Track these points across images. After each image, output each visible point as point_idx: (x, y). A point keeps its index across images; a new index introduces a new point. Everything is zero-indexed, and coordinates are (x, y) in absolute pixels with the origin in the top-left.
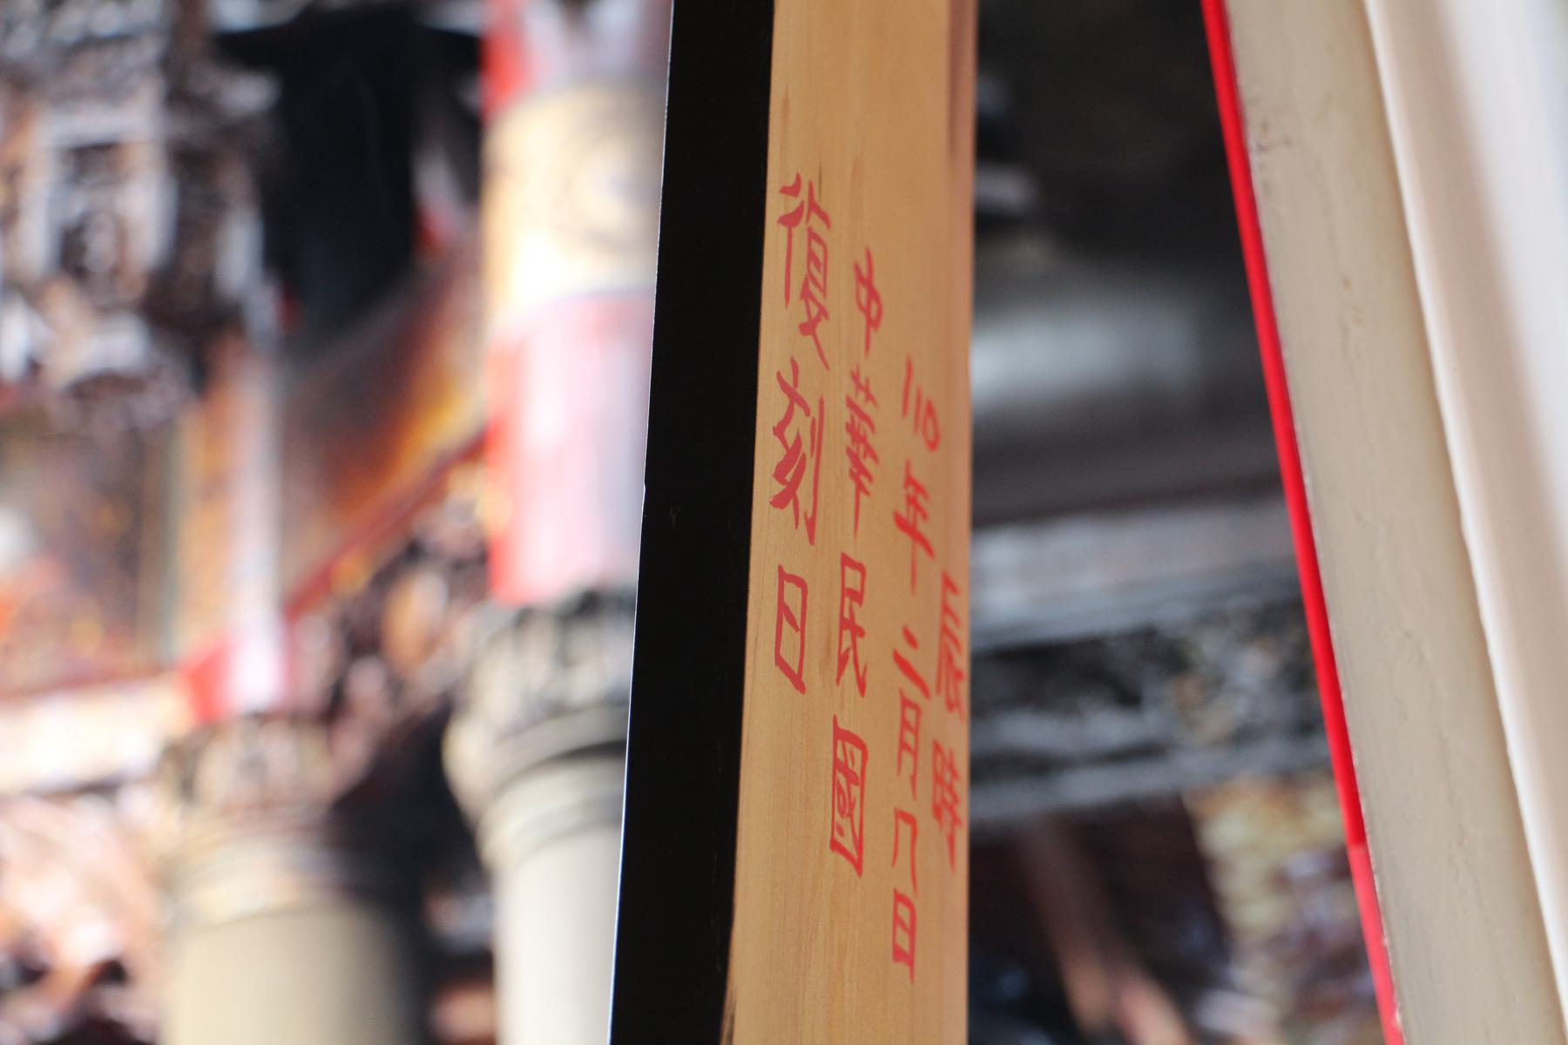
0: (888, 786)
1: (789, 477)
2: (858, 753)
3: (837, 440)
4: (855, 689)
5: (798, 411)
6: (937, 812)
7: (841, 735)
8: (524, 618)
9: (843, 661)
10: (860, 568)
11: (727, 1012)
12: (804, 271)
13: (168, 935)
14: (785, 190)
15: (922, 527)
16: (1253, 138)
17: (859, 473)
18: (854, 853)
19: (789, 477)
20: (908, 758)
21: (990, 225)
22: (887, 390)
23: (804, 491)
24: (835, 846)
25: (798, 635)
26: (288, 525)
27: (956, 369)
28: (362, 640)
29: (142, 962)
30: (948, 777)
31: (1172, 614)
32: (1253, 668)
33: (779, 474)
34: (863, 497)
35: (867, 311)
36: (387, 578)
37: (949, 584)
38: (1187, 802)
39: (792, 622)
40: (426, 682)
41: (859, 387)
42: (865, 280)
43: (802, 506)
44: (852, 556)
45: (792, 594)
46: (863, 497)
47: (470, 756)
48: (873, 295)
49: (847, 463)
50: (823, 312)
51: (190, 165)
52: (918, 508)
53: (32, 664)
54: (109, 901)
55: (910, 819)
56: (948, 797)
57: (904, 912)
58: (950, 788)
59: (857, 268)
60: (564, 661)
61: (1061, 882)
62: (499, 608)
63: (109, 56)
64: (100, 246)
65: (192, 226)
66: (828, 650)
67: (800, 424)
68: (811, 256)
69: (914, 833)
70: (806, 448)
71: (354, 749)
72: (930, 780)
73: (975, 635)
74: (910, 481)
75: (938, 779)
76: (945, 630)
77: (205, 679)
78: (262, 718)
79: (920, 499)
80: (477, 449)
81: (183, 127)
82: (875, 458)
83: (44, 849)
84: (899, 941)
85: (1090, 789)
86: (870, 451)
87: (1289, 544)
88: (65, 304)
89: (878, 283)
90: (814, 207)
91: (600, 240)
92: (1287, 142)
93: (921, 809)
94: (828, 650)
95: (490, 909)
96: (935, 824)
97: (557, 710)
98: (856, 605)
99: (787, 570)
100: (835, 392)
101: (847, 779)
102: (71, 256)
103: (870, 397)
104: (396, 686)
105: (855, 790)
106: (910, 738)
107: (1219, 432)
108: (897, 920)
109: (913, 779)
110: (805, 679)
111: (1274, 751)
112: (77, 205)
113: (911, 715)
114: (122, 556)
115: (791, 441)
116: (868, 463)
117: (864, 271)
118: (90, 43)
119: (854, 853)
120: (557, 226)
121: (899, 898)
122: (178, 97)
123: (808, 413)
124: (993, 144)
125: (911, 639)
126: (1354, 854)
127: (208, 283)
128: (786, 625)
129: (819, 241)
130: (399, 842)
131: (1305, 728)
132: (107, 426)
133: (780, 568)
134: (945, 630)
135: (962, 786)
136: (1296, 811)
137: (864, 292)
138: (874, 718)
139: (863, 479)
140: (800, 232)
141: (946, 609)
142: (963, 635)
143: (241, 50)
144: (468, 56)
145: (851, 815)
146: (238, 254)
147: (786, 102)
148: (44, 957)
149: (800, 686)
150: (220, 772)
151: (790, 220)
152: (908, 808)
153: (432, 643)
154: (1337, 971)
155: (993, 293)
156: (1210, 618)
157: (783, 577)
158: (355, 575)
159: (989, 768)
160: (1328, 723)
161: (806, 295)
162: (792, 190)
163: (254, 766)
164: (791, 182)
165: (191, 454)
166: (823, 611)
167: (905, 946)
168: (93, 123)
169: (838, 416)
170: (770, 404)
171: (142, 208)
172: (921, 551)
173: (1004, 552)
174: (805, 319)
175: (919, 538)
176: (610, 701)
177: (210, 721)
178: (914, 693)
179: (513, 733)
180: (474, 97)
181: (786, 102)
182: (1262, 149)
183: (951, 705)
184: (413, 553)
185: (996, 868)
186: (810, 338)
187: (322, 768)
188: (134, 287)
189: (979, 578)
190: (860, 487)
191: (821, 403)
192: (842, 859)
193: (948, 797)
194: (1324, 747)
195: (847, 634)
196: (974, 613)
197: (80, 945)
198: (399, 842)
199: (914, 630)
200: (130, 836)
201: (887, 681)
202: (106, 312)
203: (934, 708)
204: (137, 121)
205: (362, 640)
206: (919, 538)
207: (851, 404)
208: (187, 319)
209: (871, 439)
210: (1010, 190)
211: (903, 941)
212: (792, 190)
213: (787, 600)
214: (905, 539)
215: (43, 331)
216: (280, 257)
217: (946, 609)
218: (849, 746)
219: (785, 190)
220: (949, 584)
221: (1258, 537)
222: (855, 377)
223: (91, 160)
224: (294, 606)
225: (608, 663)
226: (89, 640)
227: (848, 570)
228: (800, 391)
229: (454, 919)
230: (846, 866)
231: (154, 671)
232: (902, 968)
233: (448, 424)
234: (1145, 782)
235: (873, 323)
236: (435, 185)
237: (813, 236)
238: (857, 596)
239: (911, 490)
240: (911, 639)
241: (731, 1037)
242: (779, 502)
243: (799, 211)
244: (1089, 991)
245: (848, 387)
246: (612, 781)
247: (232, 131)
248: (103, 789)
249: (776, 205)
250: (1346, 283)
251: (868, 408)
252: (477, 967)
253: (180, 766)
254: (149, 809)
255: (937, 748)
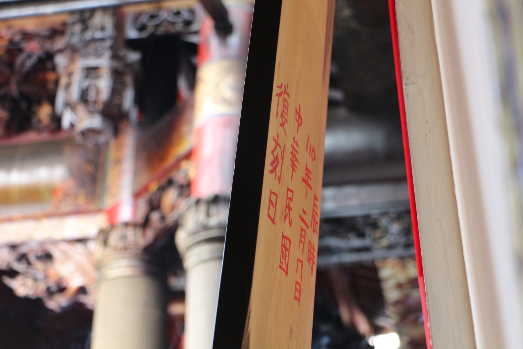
0: (296, 252)
1: (274, 165)
2: (288, 242)
3: (288, 156)
4: (289, 225)
5: (278, 147)
6: (309, 261)
7: (284, 237)
8: (198, 202)
9: (286, 217)
10: (292, 192)
11: (249, 311)
12: (282, 109)
13: (98, 281)
14: (278, 87)
15: (309, 182)
16: (404, 82)
17: (293, 166)
18: (286, 270)
19: (274, 165)
20: (302, 245)
21: (332, 104)
22: (302, 143)
23: (278, 169)
24: (281, 267)
25: (274, 209)
26: (136, 173)
27: (321, 141)
28: (154, 206)
29: (90, 288)
30: (312, 251)
31: (375, 212)
32: (395, 228)
33: (272, 164)
34: (294, 172)
35: (298, 122)
36: (162, 189)
37: (316, 198)
38: (376, 263)
39: (273, 205)
40: (171, 218)
41: (295, 142)
42: (298, 113)
43: (277, 174)
44: (290, 188)
45: (273, 197)
46: (294, 172)
47: (182, 239)
48: (300, 117)
49: (290, 162)
50: (286, 121)
51: (117, 75)
52: (309, 176)
53: (66, 207)
54: (83, 272)
55: (301, 262)
56: (312, 256)
57: (298, 287)
58: (313, 254)
59: (296, 110)
60: (208, 215)
61: (340, 283)
62: (193, 199)
63: (98, 44)
64: (92, 96)
65: (116, 91)
66: (282, 213)
67: (278, 151)
68: (284, 105)
69: (302, 265)
70: (279, 158)
71: (150, 234)
72: (307, 251)
73: (322, 214)
74: (307, 169)
75: (309, 251)
76: (314, 210)
77: (112, 213)
78: (126, 225)
79: (309, 174)
80: (189, 156)
81: (116, 64)
82: (298, 162)
83: (67, 256)
84: (296, 295)
85: (349, 258)
86: (297, 160)
87: (408, 196)
88: (81, 110)
89: (301, 114)
90: (286, 92)
91: (225, 101)
92: (414, 83)
93: (305, 259)
94: (282, 213)
95: (185, 281)
96: (308, 263)
97: (206, 228)
98: (290, 202)
99: (272, 191)
100: (289, 143)
101: (285, 249)
102: (84, 97)
103: (297, 145)
104: (163, 218)
105: (287, 253)
106: (302, 239)
107: (391, 163)
108: (296, 289)
109: (303, 251)
110: (275, 221)
111: (399, 251)
112: (86, 83)
113: (303, 233)
114: (92, 180)
115: (275, 155)
116: (296, 163)
117: (298, 111)
118: (94, 40)
119: (286, 270)
120: (214, 96)
121: (297, 283)
122: (115, 56)
123: (280, 148)
124: (334, 82)
125: (305, 212)
126: (420, 279)
127: (120, 106)
128: (271, 206)
129: (286, 101)
130: (161, 261)
131: (408, 246)
132: (90, 143)
133: (270, 190)
134: (314, 210)
135: (316, 254)
136: (404, 267)
137: (298, 116)
138: (293, 233)
139: (294, 167)
140: (281, 98)
141: (314, 205)
142: (319, 212)
143: (132, 44)
144: (194, 49)
145: (285, 259)
146: (128, 99)
147: (280, 63)
148: (64, 285)
149: (274, 223)
150: (114, 239)
151: (279, 95)
152: (301, 259)
153: (173, 207)
154: (411, 314)
155: (332, 123)
156: (385, 214)
157: (271, 192)
158: (154, 187)
159: (324, 251)
160: (415, 245)
161: (282, 116)
162: (280, 87)
163: (124, 237)
164: (280, 84)
165: (112, 153)
166: (281, 203)
167: (298, 296)
168: (92, 62)
169: (289, 150)
170: (270, 145)
171: (104, 85)
172: (308, 188)
173: (329, 192)
174: (281, 122)
175: (308, 185)
176: (220, 227)
177: (113, 226)
178: (304, 227)
179: (194, 233)
180: (195, 60)
181: (280, 63)
182: (406, 85)
183: (314, 231)
184: (170, 183)
185: (323, 277)
186: (282, 128)
187: (141, 239)
188: (100, 107)
189: (323, 199)
190: (293, 170)
191: (284, 146)
192: (282, 271)
193: (312, 256)
194: (414, 251)
195: (287, 209)
196: (321, 209)
197: (74, 282)
198: (161, 261)
199: (305, 210)
200: (90, 254)
201: (297, 223)
202: (91, 113)
203: (309, 231)
204: (104, 62)
205: (154, 206)
206: (308, 185)
207: (292, 147)
208: (113, 115)
209: (297, 157)
210: (338, 95)
211: (297, 295)
212: (280, 87)
213: (272, 199)
214: (305, 185)
215: (74, 117)
216: (139, 101)
217: (314, 205)
218: (286, 240)
219: (278, 87)
220: (316, 198)
221: (399, 193)
222: (294, 139)
223: (91, 72)
224: (137, 195)
225: (221, 215)
226: (82, 201)
227: (289, 192)
228: (279, 142)
229: (175, 283)
230: (283, 273)
231: (99, 211)
232: (297, 302)
233: (182, 149)
234: (364, 257)
235: (300, 125)
236: (182, 84)
237: (285, 100)
238: (291, 199)
239: (307, 171)
240: (305, 212)
241: (249, 318)
242: (271, 172)
243: (282, 92)
244: (345, 314)
245: (292, 142)
246: (221, 248)
247: (129, 66)
248: (82, 241)
249: (275, 91)
250: (427, 123)
251: (297, 148)
252: (180, 296)
253: (104, 236)
254: (94, 246)
255: (310, 243)
